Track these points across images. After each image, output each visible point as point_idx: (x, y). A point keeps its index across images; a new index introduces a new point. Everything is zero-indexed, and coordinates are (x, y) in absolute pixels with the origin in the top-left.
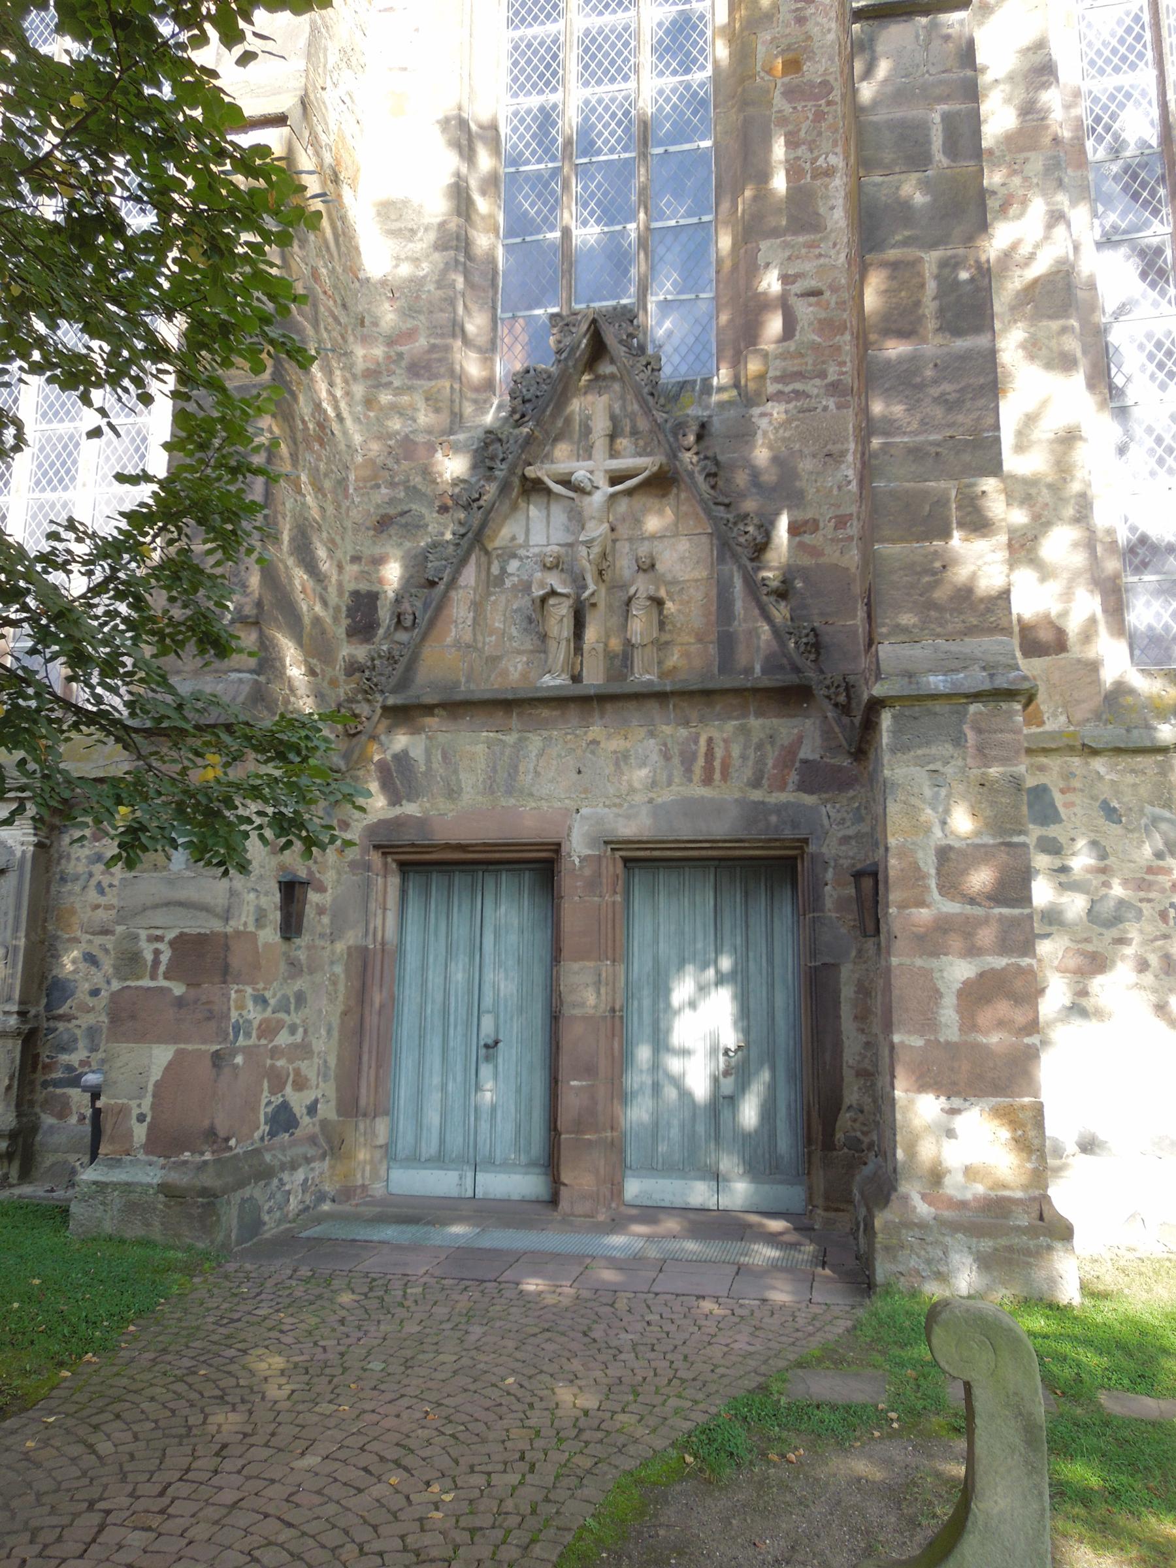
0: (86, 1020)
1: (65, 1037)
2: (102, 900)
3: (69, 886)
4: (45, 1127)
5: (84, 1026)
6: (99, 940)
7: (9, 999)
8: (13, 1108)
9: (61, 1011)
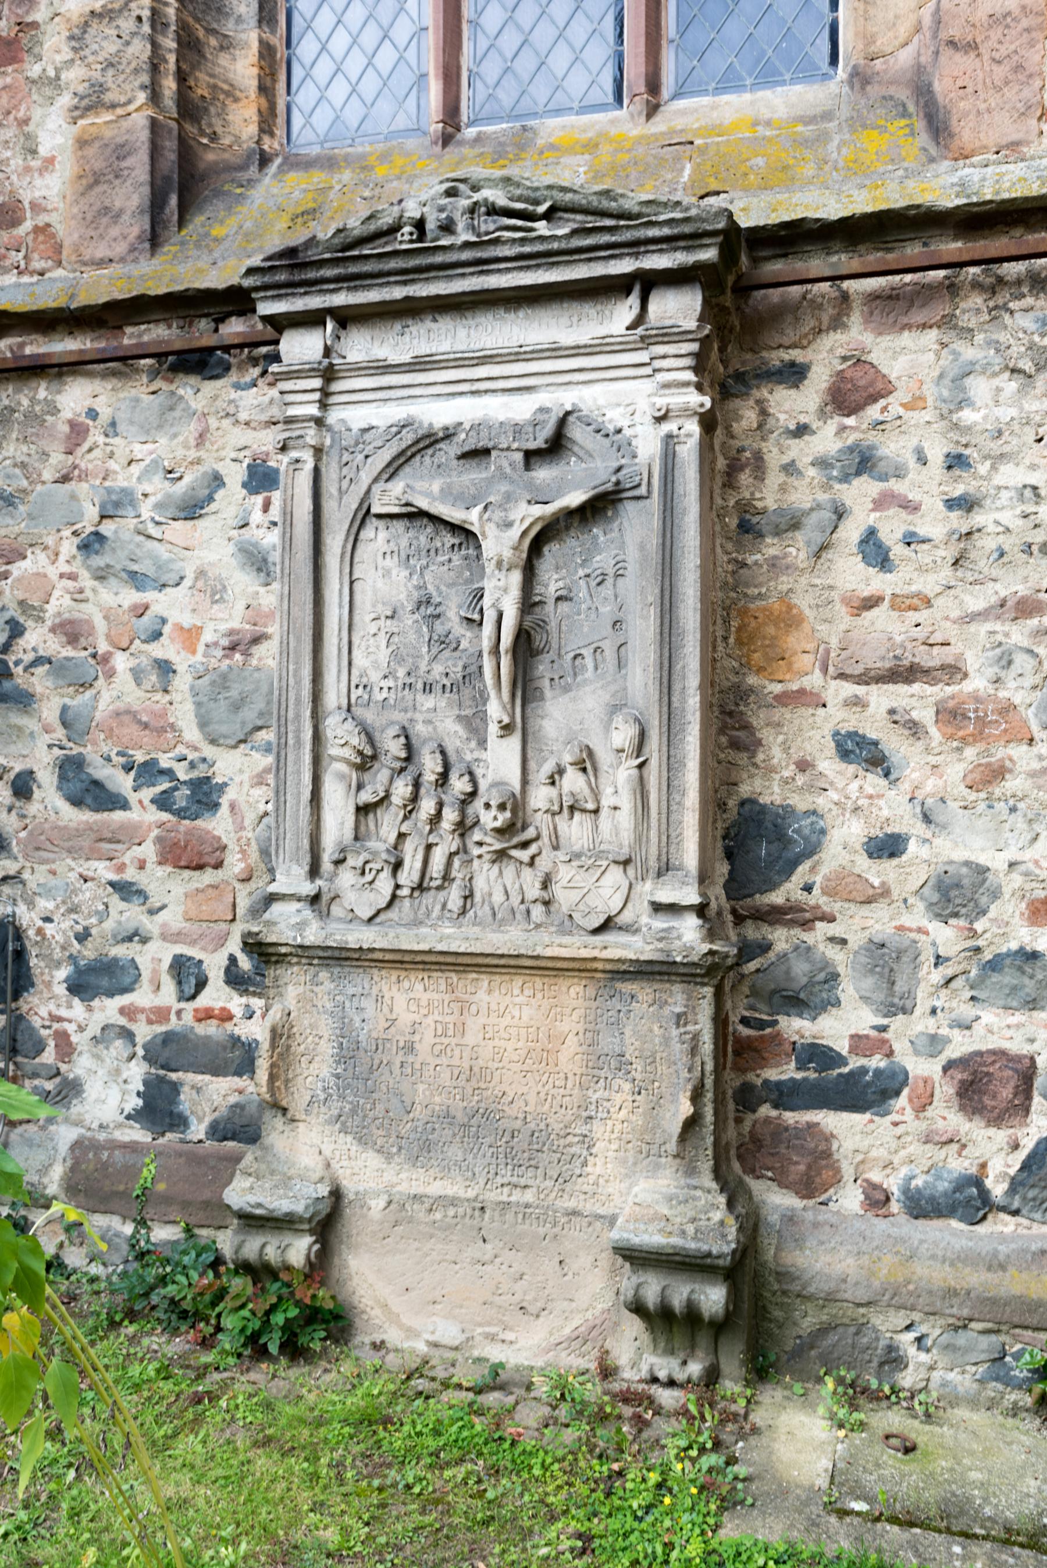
0: (860, 925)
1: (800, 969)
2: (879, 583)
3: (771, 547)
4: (774, 1218)
5: (856, 941)
6: (881, 698)
7: (665, 869)
8: (707, 1180)
9: (777, 898)
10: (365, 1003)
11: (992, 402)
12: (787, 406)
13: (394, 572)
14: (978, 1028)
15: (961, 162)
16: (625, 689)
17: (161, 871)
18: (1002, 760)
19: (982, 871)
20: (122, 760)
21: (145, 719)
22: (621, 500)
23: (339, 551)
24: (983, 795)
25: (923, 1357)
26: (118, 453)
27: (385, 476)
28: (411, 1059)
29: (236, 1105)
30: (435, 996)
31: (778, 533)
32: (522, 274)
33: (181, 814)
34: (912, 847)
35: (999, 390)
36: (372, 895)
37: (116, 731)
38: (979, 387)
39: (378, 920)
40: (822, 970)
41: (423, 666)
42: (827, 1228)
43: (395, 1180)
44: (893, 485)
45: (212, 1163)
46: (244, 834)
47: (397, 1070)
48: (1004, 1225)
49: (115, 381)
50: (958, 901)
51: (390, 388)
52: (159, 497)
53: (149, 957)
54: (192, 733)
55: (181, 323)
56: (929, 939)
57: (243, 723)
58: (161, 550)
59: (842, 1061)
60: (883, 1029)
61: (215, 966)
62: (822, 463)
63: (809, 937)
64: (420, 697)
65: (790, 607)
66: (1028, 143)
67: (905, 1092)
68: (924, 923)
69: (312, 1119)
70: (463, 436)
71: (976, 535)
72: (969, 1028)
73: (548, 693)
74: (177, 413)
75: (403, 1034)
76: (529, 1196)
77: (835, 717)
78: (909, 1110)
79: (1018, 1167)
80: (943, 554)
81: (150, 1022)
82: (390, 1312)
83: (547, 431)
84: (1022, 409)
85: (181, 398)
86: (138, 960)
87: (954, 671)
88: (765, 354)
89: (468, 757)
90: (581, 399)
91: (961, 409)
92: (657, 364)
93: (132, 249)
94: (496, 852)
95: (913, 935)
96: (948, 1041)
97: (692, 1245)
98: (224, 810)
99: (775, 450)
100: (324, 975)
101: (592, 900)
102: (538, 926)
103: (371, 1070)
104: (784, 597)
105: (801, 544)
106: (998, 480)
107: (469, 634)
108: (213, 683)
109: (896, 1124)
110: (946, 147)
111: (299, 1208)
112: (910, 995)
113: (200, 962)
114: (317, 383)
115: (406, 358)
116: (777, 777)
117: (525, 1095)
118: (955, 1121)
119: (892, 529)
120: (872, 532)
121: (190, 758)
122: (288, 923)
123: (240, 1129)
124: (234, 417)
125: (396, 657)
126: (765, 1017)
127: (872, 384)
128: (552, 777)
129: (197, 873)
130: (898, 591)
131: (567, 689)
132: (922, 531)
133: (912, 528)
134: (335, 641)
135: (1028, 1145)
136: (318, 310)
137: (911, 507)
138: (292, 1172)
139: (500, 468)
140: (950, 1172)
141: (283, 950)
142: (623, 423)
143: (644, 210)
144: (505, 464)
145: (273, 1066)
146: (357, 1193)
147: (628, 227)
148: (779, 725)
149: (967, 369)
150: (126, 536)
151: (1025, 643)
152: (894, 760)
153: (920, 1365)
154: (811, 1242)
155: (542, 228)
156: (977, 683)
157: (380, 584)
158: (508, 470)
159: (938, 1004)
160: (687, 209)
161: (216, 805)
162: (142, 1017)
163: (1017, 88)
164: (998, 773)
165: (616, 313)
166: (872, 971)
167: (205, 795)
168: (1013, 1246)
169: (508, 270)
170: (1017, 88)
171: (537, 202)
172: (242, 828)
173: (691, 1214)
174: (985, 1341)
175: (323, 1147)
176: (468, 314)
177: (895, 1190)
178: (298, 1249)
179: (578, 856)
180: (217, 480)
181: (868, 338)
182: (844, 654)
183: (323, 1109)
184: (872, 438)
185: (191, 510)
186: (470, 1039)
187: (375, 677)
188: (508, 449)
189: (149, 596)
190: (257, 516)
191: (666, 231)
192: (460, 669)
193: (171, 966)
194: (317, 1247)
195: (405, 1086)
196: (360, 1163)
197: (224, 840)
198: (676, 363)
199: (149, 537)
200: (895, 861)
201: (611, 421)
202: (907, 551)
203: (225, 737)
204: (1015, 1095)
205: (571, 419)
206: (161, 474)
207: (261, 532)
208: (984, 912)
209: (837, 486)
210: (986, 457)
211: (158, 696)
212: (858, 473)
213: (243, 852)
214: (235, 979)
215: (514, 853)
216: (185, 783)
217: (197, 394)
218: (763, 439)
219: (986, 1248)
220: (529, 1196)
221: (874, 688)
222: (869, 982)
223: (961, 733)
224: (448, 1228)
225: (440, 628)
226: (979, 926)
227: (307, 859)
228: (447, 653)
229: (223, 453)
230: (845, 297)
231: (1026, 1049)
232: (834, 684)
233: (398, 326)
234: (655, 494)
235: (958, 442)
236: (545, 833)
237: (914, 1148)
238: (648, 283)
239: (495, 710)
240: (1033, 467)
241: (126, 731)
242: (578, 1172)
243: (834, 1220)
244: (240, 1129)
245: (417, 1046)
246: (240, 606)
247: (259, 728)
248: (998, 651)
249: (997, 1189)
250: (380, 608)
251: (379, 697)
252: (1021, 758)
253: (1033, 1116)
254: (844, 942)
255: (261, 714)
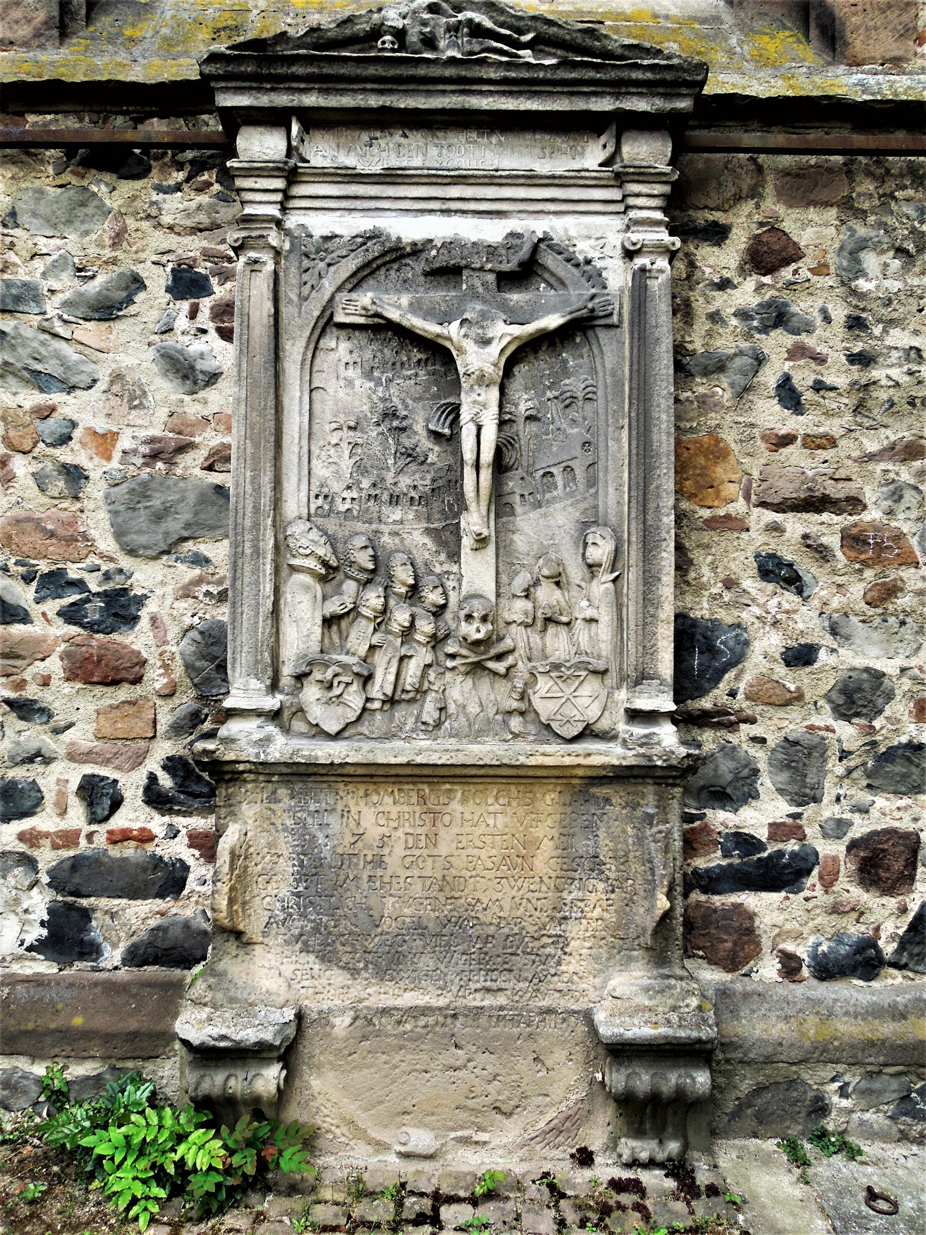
0: (776, 726)
1: (726, 767)
6: (796, 525)
7: (642, 678)
9: (706, 703)
10: (329, 819)
11: (879, 275)
12: (711, 261)
13: (358, 383)
14: (874, 812)
15: (854, 69)
16: (596, 507)
17: (67, 688)
18: (895, 580)
19: (878, 676)
20: (21, 569)
21: (50, 527)
22: (593, 327)
23: (300, 358)
24: (880, 611)
25: (845, 1103)
26: (19, 245)
27: (349, 286)
28: (379, 872)
29: (158, 929)
30: (406, 808)
31: (706, 372)
32: (503, 99)
33: (93, 627)
34: (823, 655)
35: (886, 265)
36: (340, 709)
37: (16, 539)
38: (871, 261)
39: (346, 734)
40: (745, 766)
41: (390, 477)
42: (756, 997)
43: (363, 995)
44: (804, 338)
45: (134, 991)
46: (168, 648)
47: (365, 885)
48: (894, 979)
49: (15, 169)
50: (860, 703)
51: (356, 198)
52: (68, 295)
53: (52, 779)
54: (106, 543)
55: (95, 118)
56: (836, 736)
57: (167, 534)
58: (68, 350)
59: (758, 846)
60: (798, 816)
61: (132, 784)
62: (743, 315)
63: (733, 738)
64: (386, 510)
65: (718, 441)
66: (907, 60)
67: (815, 872)
68: (831, 722)
69: (270, 941)
70: (434, 252)
71: (871, 388)
72: (867, 812)
73: (519, 509)
74: (90, 210)
75: (370, 847)
76: (501, 1000)
77: (756, 540)
78: (818, 886)
79: (905, 928)
80: (846, 401)
81: (55, 847)
82: (358, 1128)
83: (524, 253)
84: (906, 284)
85: (94, 194)
86: (40, 782)
87: (855, 503)
88: (691, 212)
89: (438, 569)
90: (552, 228)
91: (857, 278)
92: (631, 201)
93: (37, 35)
94: (472, 663)
95: (821, 733)
96: (850, 824)
97: (682, 1034)
98: (144, 623)
99: (701, 300)
100: (283, 792)
101: (569, 711)
102: (516, 736)
103: (335, 887)
104: (712, 433)
105: (725, 385)
106: (889, 341)
107: (436, 448)
108: (132, 491)
109: (807, 899)
110: (842, 53)
111: (268, 1035)
112: (819, 786)
113: (115, 781)
114: (280, 184)
115: (377, 169)
116: (707, 593)
117: (499, 899)
118: (857, 894)
119: (803, 378)
120: (787, 378)
121: (104, 568)
122: (244, 740)
123: (173, 952)
124: (162, 219)
125: (360, 468)
126: (694, 812)
127: (785, 248)
128: (527, 590)
129: (111, 689)
130: (809, 431)
131: (538, 505)
132: (829, 380)
133: (819, 377)
134: (296, 449)
135: (914, 908)
136: (286, 109)
137: (820, 360)
138: (252, 998)
139: (472, 287)
140: (849, 937)
141: (241, 767)
142: (593, 254)
143: (626, 53)
144: (478, 283)
145: (232, 889)
146: (320, 1012)
147: (614, 66)
148: (708, 546)
149: (863, 244)
150: (29, 333)
151: (912, 482)
152: (807, 578)
153: (841, 1110)
154: (744, 1012)
155: (527, 55)
156: (873, 515)
157: (341, 394)
158: (480, 290)
159: (841, 792)
160: (669, 58)
161: (135, 619)
162: (47, 842)
163: (897, 12)
164: (891, 591)
165: (588, 150)
166: (788, 767)
167: (121, 607)
168: (908, 996)
169: (491, 93)
170: (897, 12)
171: (521, 32)
172: (165, 642)
173: (671, 1002)
174: (894, 1084)
175: (283, 968)
176: (440, 134)
177: (805, 956)
178: (268, 1079)
179: (556, 667)
180: (137, 283)
181: (781, 209)
182: (764, 485)
183: (283, 930)
184: (786, 296)
185: (106, 310)
186: (443, 849)
187: (336, 487)
188: (481, 269)
189: (56, 398)
190: (182, 322)
191: (649, 75)
192: (428, 482)
193: (81, 788)
194: (284, 1072)
195: (373, 901)
196: (324, 981)
197: (145, 655)
198: (648, 202)
199: (56, 336)
200: (808, 669)
201: (581, 252)
202: (816, 398)
203: (145, 547)
204: (905, 867)
205: (543, 246)
206: (71, 271)
207: (186, 339)
208: (880, 712)
209: (757, 336)
210: (879, 321)
211: (66, 504)
212: (775, 326)
213: (166, 666)
214: (155, 798)
215: (491, 665)
216: (98, 594)
217: (112, 193)
218: (691, 289)
219: (885, 1000)
220: (501, 1000)
221: (790, 515)
222: (784, 776)
223: (863, 557)
224: (419, 1038)
225: (407, 442)
226: (877, 724)
227: (270, 672)
228: (413, 467)
229: (143, 256)
230: (760, 169)
231: (910, 827)
232: (756, 511)
233: (365, 137)
234: (626, 325)
235: (856, 307)
236: (521, 644)
237: (821, 919)
238: (626, 124)
239: (474, 521)
240: (916, 333)
241: (27, 539)
242: (553, 971)
243: (760, 989)
244: (173, 952)
245: (386, 859)
246: (162, 414)
247: (185, 539)
248: (891, 487)
249: (888, 948)
250: (341, 419)
251: (343, 507)
252: (909, 579)
253: (918, 885)
254: (763, 741)
255: (188, 526)
